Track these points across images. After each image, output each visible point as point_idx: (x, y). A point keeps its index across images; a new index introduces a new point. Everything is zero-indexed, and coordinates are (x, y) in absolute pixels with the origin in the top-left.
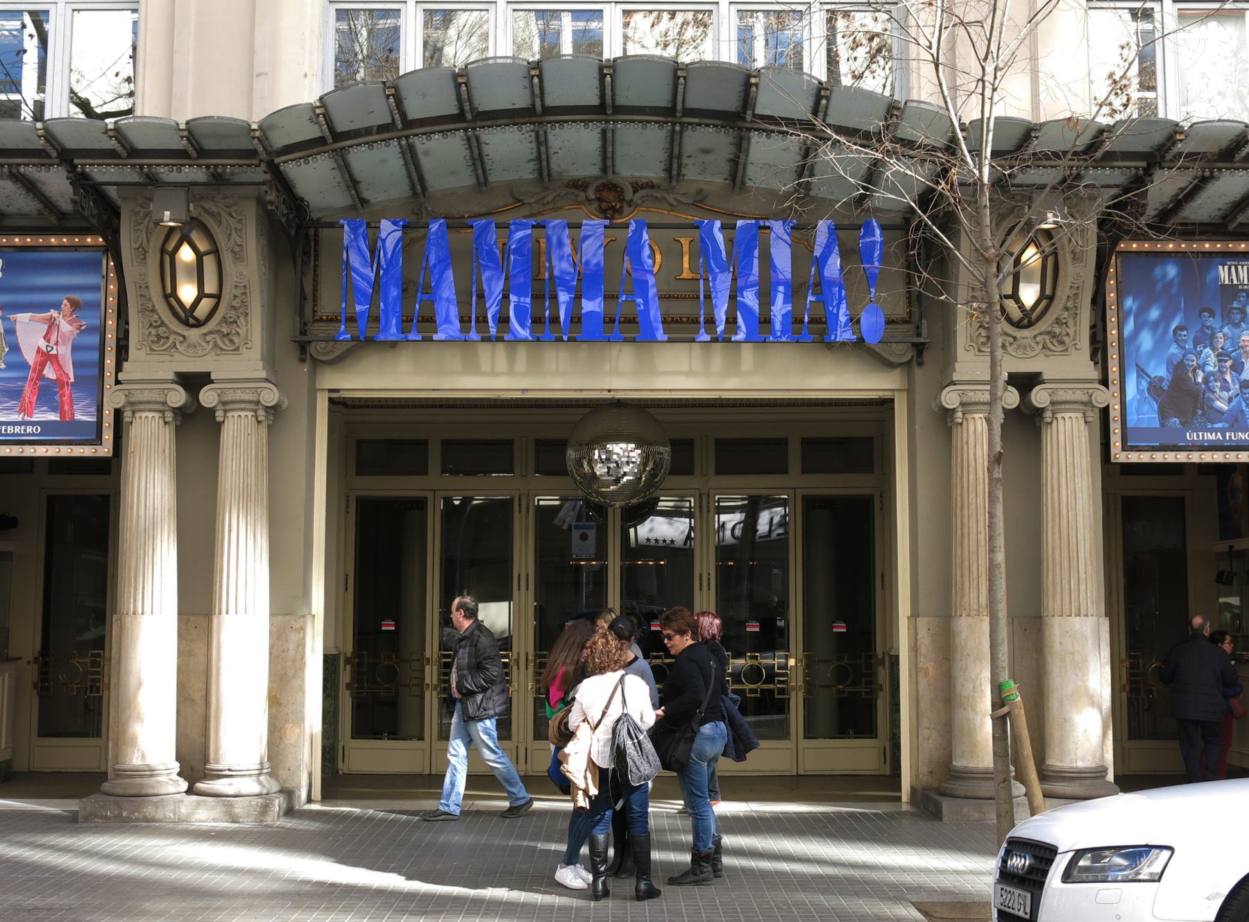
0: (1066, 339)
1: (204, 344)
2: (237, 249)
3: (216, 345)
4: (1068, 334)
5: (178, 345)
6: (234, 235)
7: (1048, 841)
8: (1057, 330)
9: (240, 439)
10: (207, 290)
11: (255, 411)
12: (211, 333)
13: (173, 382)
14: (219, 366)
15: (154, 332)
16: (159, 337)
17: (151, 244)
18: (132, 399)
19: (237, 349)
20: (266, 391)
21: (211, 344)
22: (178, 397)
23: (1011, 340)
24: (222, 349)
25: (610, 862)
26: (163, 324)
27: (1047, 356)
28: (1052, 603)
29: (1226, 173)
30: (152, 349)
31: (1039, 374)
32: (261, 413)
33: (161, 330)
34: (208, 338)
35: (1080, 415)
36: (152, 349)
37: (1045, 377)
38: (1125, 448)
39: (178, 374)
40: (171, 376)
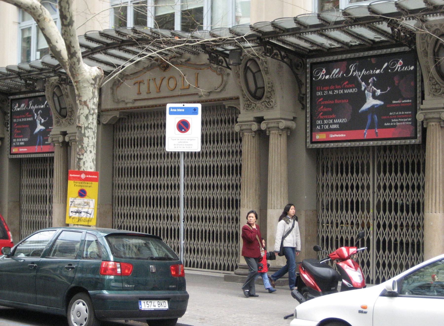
1: (262, 106)
2: (266, 69)
9: (277, 144)
10: (258, 86)
11: (440, 122)
12: (264, 102)
14: (267, 115)
15: (434, 87)
17: (429, 48)
18: (426, 117)
19: (272, 107)
20: (254, 125)
22: (255, 127)
24: (268, 108)
25: (127, 323)
26: (437, 83)
28: (269, 205)
31: (66, 132)
32: (253, 133)
35: (438, 124)
36: (434, 95)
37: (264, 118)
38: (415, 137)
39: (256, 118)
40: (59, 133)
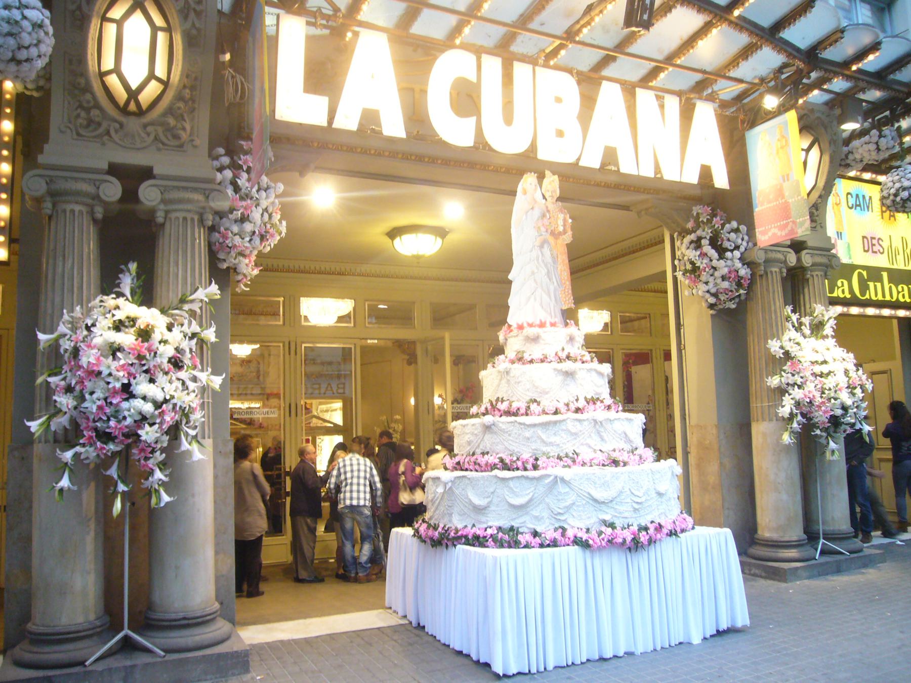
0: (181, 132)
1: (143, 135)
3: (156, 139)
4: (184, 129)
5: (112, 132)
6: (192, 15)
7: (713, 373)
8: (172, 121)
13: (789, 247)
16: (90, 122)
21: (152, 137)
23: (117, 126)
24: (163, 144)
27: (159, 150)
29: (744, 62)
30: (78, 134)
33: (95, 113)
34: (150, 129)
36: (78, 134)
37: (156, 171)
